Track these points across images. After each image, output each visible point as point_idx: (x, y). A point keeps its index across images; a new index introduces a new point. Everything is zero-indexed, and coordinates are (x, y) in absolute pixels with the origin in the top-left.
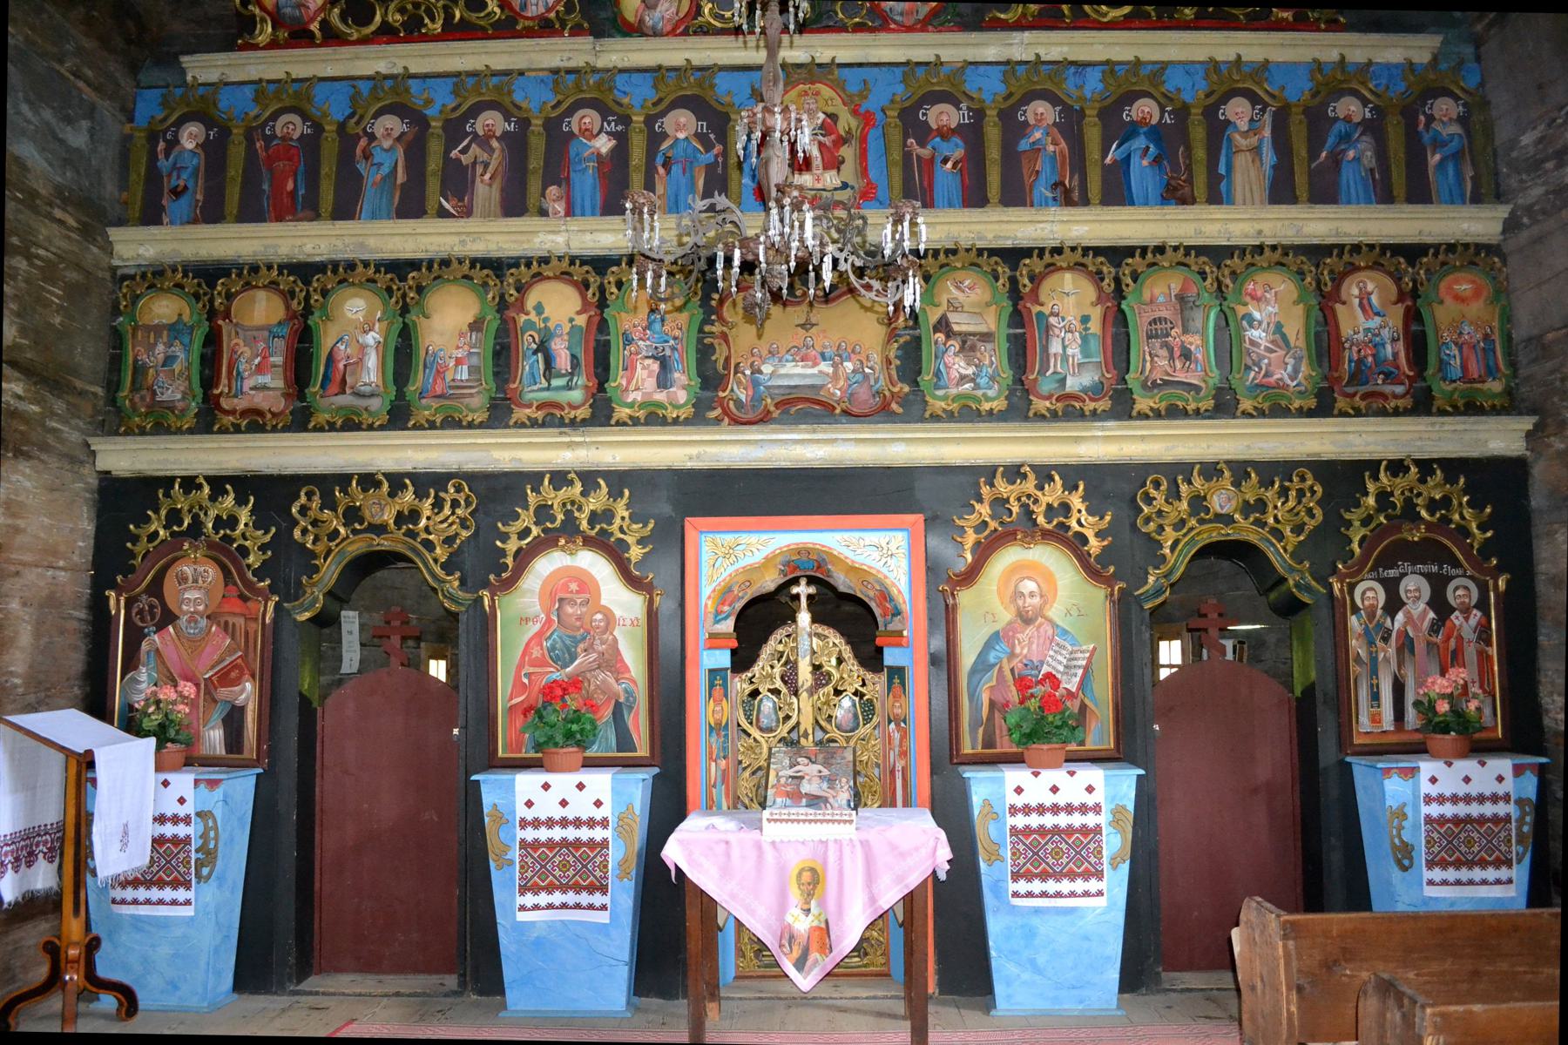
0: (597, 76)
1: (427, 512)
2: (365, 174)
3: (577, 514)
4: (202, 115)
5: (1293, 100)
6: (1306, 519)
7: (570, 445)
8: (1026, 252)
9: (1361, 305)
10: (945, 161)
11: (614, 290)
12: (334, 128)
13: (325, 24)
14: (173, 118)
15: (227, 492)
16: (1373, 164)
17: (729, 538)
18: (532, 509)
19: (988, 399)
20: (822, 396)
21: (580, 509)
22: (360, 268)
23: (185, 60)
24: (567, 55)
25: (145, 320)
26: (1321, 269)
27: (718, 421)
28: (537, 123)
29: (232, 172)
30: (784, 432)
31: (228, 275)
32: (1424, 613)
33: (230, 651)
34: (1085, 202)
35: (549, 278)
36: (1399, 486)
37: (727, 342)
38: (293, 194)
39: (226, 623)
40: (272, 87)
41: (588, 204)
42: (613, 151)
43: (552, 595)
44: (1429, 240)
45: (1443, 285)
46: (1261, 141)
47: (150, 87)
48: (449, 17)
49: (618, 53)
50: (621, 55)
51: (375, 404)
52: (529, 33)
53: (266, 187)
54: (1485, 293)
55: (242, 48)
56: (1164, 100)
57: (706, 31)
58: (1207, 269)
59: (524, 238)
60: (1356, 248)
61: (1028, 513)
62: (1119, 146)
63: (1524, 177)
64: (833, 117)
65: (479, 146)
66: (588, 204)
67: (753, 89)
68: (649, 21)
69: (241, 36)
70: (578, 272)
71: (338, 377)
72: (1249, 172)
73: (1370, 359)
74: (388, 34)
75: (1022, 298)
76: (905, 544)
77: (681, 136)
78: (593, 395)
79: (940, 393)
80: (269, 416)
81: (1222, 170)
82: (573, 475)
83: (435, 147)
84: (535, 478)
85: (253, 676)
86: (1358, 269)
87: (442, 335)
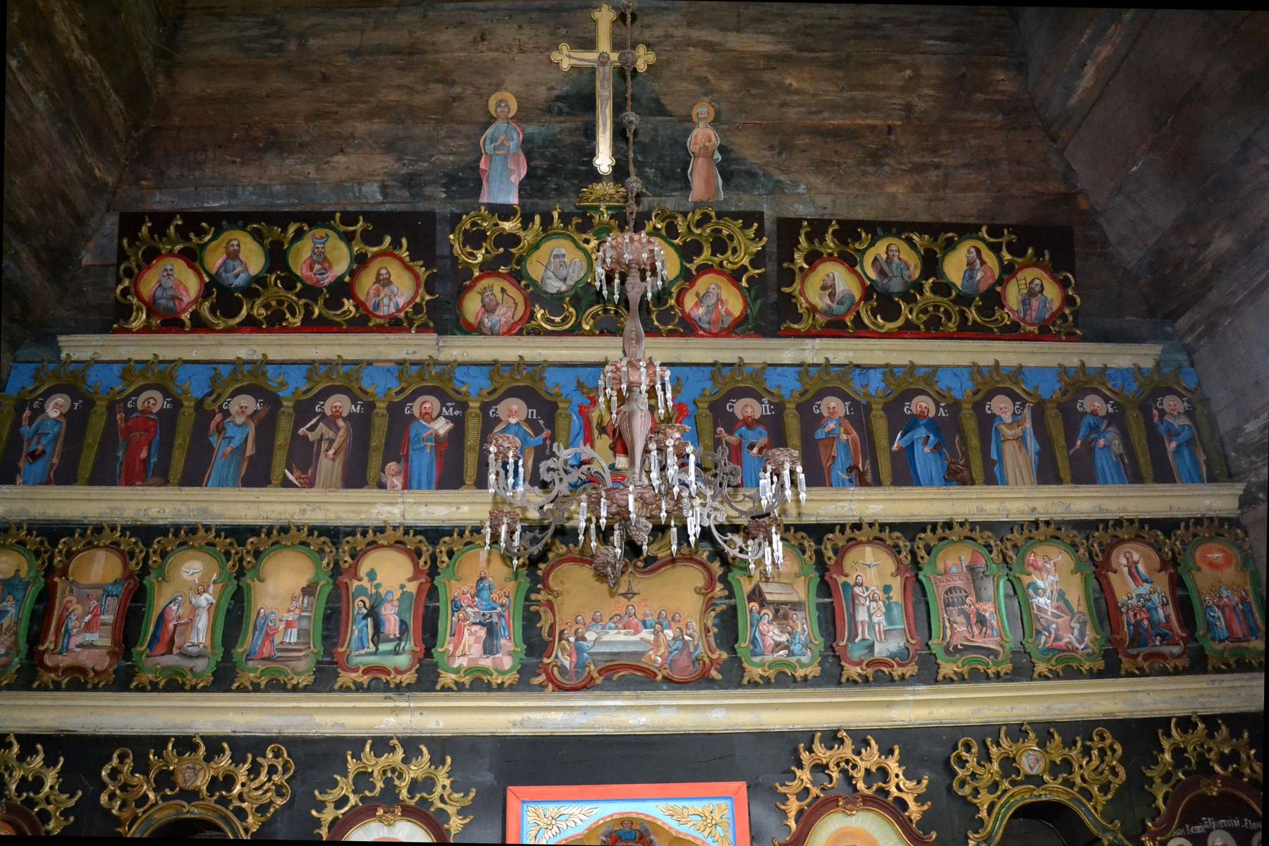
0: (439, 368)
1: (242, 779)
3: (397, 782)
4: (70, 389)
5: (1047, 396)
6: (1110, 777)
7: (394, 711)
8: (830, 528)
10: (751, 447)
11: (445, 559)
12: (192, 404)
13: (195, 316)
15: (37, 753)
16: (1121, 450)
17: (552, 809)
18: (351, 776)
19: (803, 666)
20: (644, 662)
21: (400, 777)
22: (201, 532)
23: (62, 339)
24: (412, 349)
26: (1093, 542)
27: (542, 687)
28: (381, 406)
29: (89, 440)
30: (605, 698)
31: (72, 535)
34: (878, 482)
35: (383, 546)
36: (1191, 742)
38: (146, 461)
40: (139, 366)
42: (450, 432)
44: (1180, 515)
46: (1024, 431)
47: (27, 362)
48: (308, 312)
49: (458, 349)
50: (461, 350)
51: (200, 665)
52: (380, 329)
53: (120, 454)
54: (1234, 561)
55: (115, 332)
56: (938, 398)
57: (538, 332)
58: (992, 543)
59: (363, 508)
60: (1119, 523)
61: (849, 779)
62: (903, 436)
63: (1253, 458)
66: (424, 479)
67: (578, 382)
69: (116, 321)
70: (412, 541)
71: (167, 637)
72: (1017, 457)
73: (1146, 622)
75: (828, 570)
76: (728, 814)
77: (513, 421)
78: (420, 660)
79: (757, 659)
80: (92, 674)
81: (994, 456)
82: (395, 742)
84: (355, 744)
86: (1122, 541)
87: (274, 598)
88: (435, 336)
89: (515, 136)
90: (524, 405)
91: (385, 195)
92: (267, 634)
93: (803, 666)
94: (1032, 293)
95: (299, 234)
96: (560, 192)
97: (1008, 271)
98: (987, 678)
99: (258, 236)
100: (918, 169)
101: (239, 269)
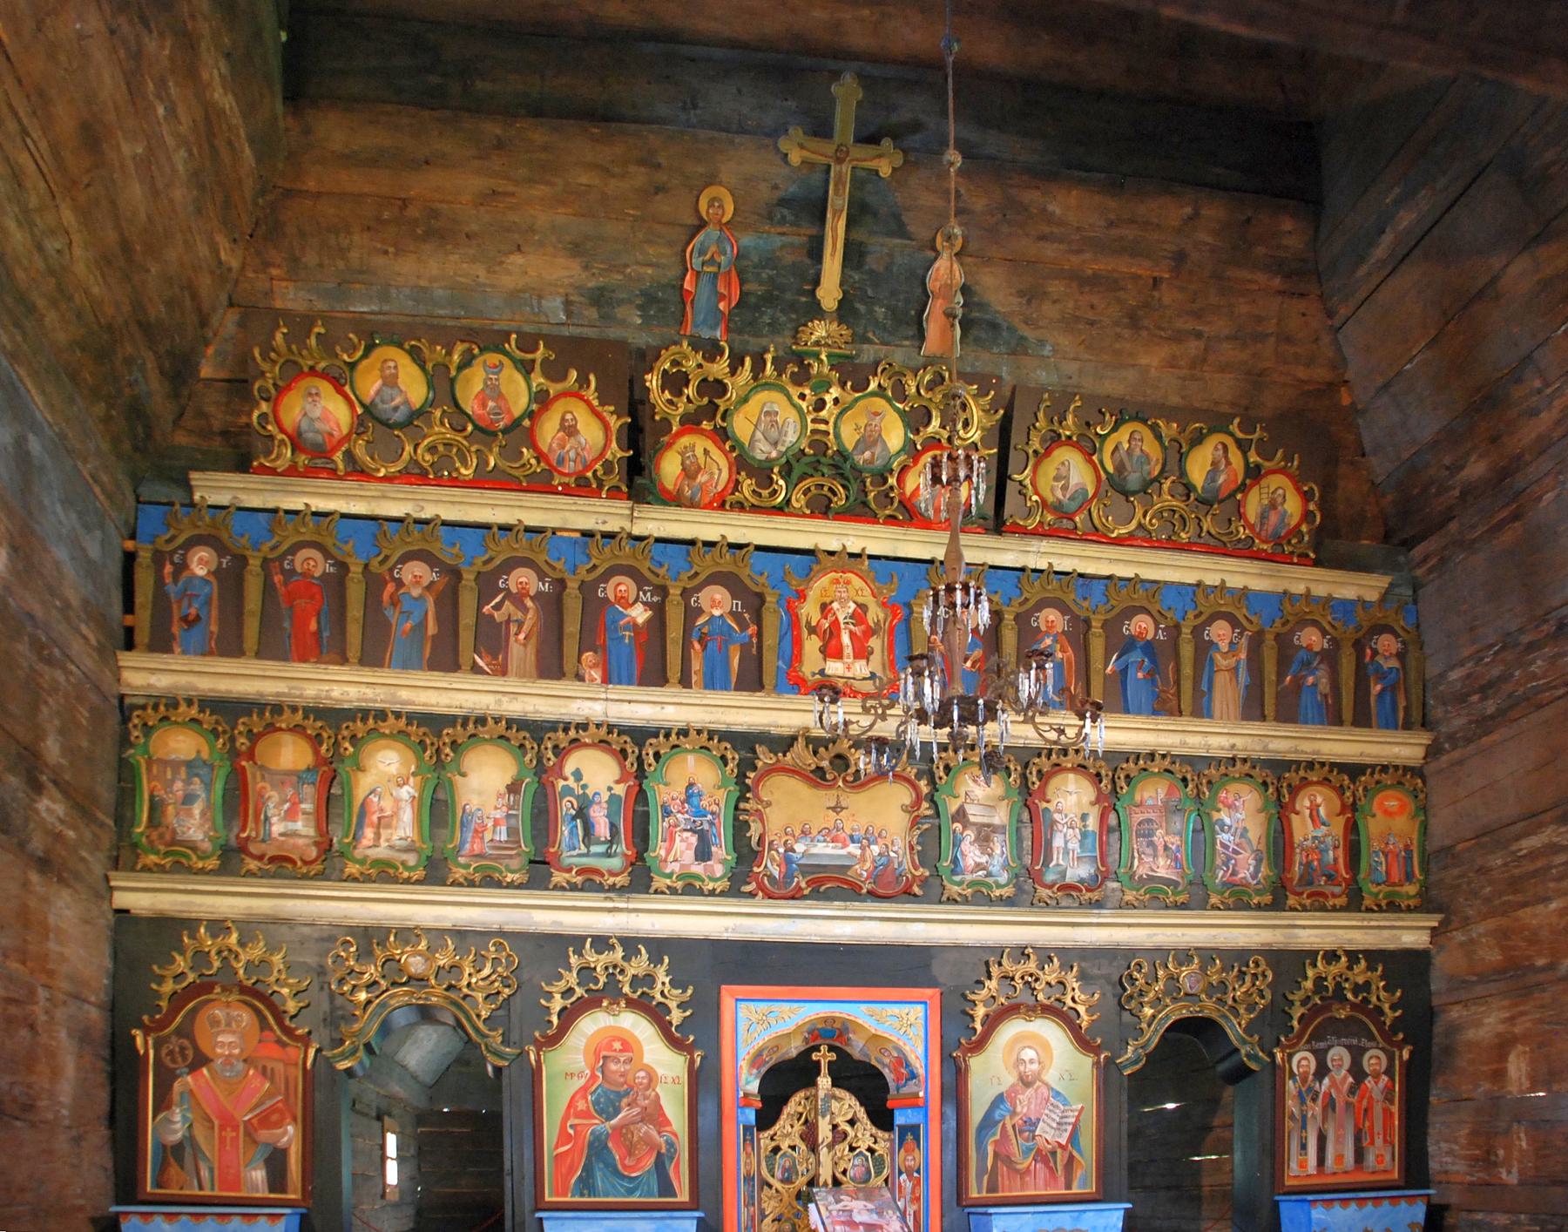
2: (393, 622)
9: (1311, 815)
14: (180, 540)
16: (1327, 690)
17: (763, 1006)
19: (999, 886)
23: (196, 478)
25: (159, 754)
26: (1280, 781)
27: (752, 895)
32: (1345, 1078)
33: (270, 1094)
37: (762, 821)
38: (318, 634)
39: (264, 1068)
41: (624, 673)
42: (649, 621)
43: (597, 1053)
44: (1368, 760)
45: (1376, 801)
46: (1238, 662)
49: (657, 522)
51: (411, 859)
53: (286, 624)
57: (740, 507)
64: (862, 607)
65: (513, 603)
66: (624, 673)
68: (688, 492)
72: (1226, 691)
74: (416, 475)
79: (957, 878)
83: (468, 600)
84: (577, 941)
85: (295, 1119)
88: (630, 504)
89: (728, 249)
90: (729, 596)
91: (569, 314)
92: (476, 831)
93: (999, 886)
94: (1273, 505)
95: (467, 362)
96: (775, 327)
97: (1254, 474)
98: (1167, 907)
99: (416, 356)
100: (1178, 337)
101: (398, 401)
